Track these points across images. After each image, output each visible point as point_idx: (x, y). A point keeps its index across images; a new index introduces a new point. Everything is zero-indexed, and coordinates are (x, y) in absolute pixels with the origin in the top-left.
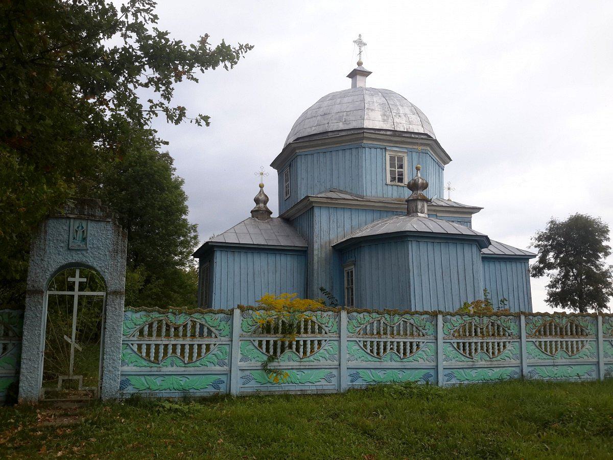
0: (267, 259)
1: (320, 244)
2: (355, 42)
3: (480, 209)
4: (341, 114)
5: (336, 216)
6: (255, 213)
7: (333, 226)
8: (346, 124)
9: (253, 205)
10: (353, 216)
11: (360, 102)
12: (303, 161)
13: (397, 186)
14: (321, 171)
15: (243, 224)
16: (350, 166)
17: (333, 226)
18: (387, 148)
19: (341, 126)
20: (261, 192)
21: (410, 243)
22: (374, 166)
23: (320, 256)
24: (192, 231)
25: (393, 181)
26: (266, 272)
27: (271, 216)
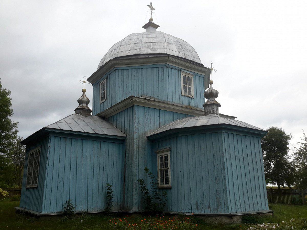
0: (108, 145)
1: (138, 134)
2: (148, 6)
4: (149, 44)
5: (149, 114)
6: (78, 111)
7: (148, 121)
8: (154, 50)
9: (77, 105)
10: (161, 115)
11: (162, 38)
12: (120, 74)
14: (134, 82)
15: (70, 117)
16: (157, 79)
17: (148, 121)
18: (182, 70)
19: (150, 52)
20: (84, 95)
21: (223, 133)
22: (173, 81)
23: (138, 144)
24: (14, 127)
26: (92, 156)
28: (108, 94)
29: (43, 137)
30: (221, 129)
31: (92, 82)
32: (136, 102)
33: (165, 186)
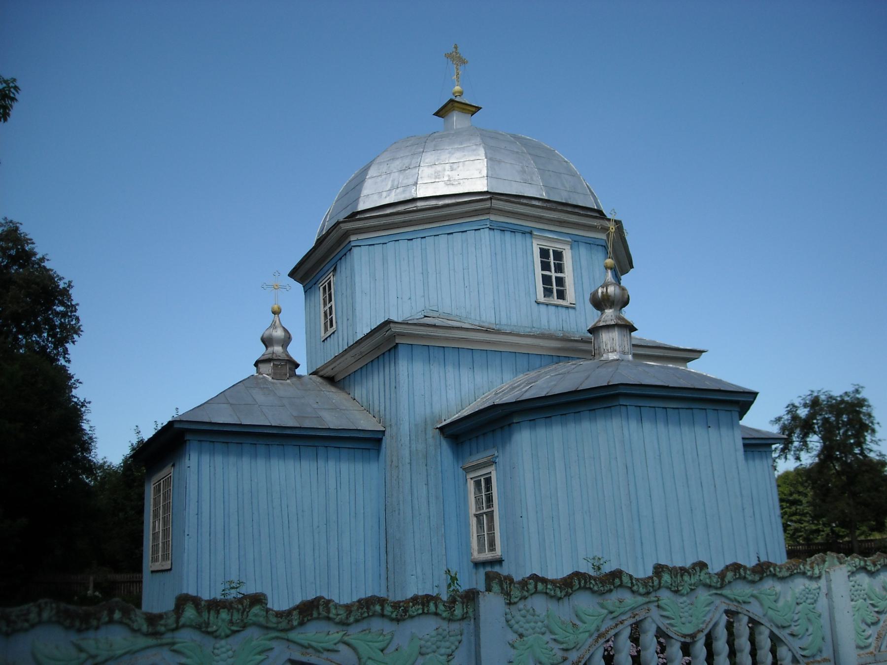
3: (701, 352)
9: (260, 351)
13: (557, 306)
25: (549, 296)
27: (298, 371)
28: (340, 314)
29: (168, 444)
30: (511, 414)
31: (301, 281)
32: (402, 335)
33: (487, 555)
